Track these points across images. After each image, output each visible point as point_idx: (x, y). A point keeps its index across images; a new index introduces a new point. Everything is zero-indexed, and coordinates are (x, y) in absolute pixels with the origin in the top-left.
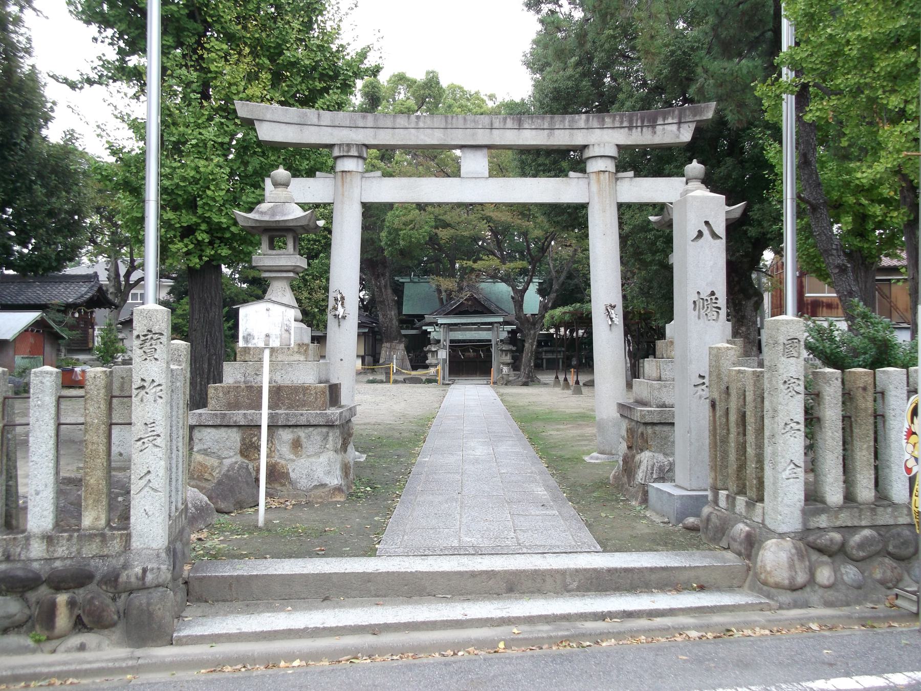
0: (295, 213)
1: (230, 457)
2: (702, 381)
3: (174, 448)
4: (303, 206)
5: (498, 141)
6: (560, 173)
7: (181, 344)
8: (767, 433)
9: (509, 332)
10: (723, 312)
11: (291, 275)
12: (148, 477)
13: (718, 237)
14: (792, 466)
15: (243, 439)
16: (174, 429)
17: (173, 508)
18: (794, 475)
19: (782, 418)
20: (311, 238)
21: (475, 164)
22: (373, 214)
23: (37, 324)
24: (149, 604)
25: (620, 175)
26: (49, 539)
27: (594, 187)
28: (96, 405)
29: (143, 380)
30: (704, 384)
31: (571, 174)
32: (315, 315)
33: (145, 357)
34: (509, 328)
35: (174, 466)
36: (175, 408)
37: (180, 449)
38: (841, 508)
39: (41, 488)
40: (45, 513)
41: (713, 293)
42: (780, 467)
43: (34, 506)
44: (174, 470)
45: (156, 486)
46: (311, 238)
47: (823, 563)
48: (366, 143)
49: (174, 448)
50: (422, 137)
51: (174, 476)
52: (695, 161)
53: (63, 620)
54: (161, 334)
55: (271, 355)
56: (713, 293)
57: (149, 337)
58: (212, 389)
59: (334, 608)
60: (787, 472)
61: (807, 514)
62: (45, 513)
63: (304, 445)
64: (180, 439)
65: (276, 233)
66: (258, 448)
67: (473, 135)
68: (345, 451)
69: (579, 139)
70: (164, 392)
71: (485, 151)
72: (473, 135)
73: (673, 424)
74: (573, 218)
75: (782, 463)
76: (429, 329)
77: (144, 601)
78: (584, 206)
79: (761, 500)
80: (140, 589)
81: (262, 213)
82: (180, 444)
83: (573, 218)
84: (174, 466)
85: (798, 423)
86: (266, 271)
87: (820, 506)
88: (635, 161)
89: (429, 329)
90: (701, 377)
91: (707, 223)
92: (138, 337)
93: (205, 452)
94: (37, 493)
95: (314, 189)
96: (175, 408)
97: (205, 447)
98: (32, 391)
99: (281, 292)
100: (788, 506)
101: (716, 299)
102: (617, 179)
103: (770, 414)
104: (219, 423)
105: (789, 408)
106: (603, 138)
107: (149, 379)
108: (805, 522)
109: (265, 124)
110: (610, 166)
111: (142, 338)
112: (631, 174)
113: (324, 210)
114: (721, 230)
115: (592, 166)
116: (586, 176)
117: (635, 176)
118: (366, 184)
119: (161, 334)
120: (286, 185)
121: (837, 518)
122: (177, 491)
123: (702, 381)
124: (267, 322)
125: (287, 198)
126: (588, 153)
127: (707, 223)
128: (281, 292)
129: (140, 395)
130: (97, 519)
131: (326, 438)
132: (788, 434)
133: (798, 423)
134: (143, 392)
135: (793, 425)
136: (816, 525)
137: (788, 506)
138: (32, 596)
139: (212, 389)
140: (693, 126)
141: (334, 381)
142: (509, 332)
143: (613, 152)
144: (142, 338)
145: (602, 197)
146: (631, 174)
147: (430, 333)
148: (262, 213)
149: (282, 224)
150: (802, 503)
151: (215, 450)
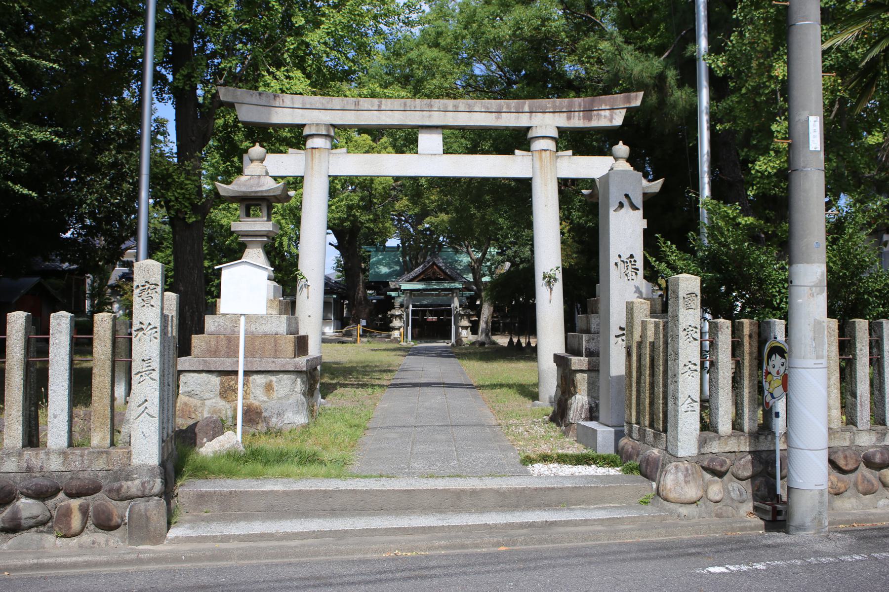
0: (268, 186)
1: (211, 399)
2: (622, 332)
3: (166, 382)
4: (275, 178)
5: (451, 122)
6: (507, 150)
7: (172, 298)
8: (670, 373)
9: (467, 298)
10: (641, 272)
11: (265, 239)
12: (145, 405)
13: (636, 209)
14: (689, 400)
15: (222, 383)
16: (166, 366)
17: (165, 435)
18: (690, 409)
19: (682, 360)
20: (283, 202)
21: (431, 142)
22: (337, 186)
23: (39, 286)
24: (146, 510)
25: (560, 153)
26: (63, 453)
27: (537, 164)
28: (103, 344)
29: (141, 323)
30: (623, 334)
31: (517, 151)
32: (285, 272)
33: (143, 303)
34: (468, 293)
35: (166, 397)
36: (167, 348)
37: (171, 383)
38: (730, 436)
39: (57, 413)
40: (62, 433)
41: (632, 256)
42: (680, 402)
43: (53, 427)
44: (166, 401)
45: (151, 413)
46: (283, 202)
47: (714, 482)
48: (334, 123)
49: (166, 382)
50: (384, 118)
51: (166, 406)
52: (621, 142)
53: (76, 521)
54: (157, 285)
55: (246, 323)
56: (632, 256)
57: (146, 287)
58: (196, 339)
59: (301, 518)
60: (685, 406)
61: (702, 443)
62: (62, 433)
63: (276, 389)
64: (171, 376)
65: (252, 203)
66: (235, 391)
67: (430, 116)
68: (312, 395)
69: (523, 121)
70: (159, 333)
71: (440, 131)
72: (430, 116)
73: (598, 371)
74: (520, 191)
75: (682, 398)
76: (393, 294)
77: (142, 508)
78: (531, 179)
79: (665, 431)
80: (139, 497)
81: (240, 185)
82: (171, 380)
83: (520, 191)
84: (166, 397)
85: (695, 365)
86: (243, 236)
87: (712, 434)
88: (577, 141)
89: (393, 294)
90: (621, 329)
91: (627, 196)
92: (138, 286)
93: (189, 394)
94: (55, 417)
95: (287, 163)
96: (167, 348)
97: (190, 389)
98: (51, 332)
99: (255, 255)
100: (686, 434)
101: (635, 261)
102: (558, 157)
103: (673, 357)
104: (201, 369)
105: (688, 351)
106: (545, 120)
107: (146, 323)
108: (699, 451)
109: (245, 107)
110: (551, 145)
111: (141, 288)
112: (570, 152)
113: (297, 182)
114: (638, 201)
115: (537, 145)
116: (530, 153)
117: (574, 154)
118: (333, 159)
119: (157, 285)
120: (262, 160)
121: (726, 444)
122: (168, 420)
123: (622, 332)
124: (245, 287)
125: (263, 170)
126: (531, 134)
127: (627, 196)
128: (255, 255)
129: (139, 336)
130: (103, 439)
131: (294, 382)
132: (687, 374)
133: (695, 365)
134: (141, 333)
135: (690, 366)
136: (709, 450)
137: (686, 434)
138: (50, 503)
139: (196, 339)
140: (624, 112)
141: (302, 333)
142: (467, 298)
143: (555, 134)
144: (141, 288)
145: (544, 170)
146: (570, 152)
147: (394, 298)
148: (239, 185)
149: (259, 194)
150: (698, 432)
151: (198, 393)
